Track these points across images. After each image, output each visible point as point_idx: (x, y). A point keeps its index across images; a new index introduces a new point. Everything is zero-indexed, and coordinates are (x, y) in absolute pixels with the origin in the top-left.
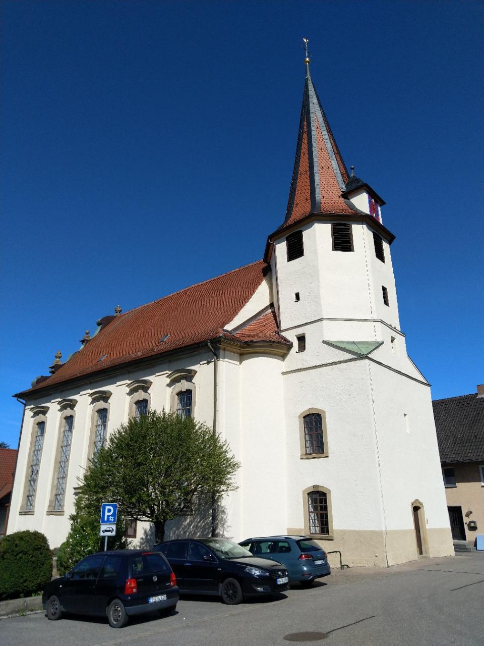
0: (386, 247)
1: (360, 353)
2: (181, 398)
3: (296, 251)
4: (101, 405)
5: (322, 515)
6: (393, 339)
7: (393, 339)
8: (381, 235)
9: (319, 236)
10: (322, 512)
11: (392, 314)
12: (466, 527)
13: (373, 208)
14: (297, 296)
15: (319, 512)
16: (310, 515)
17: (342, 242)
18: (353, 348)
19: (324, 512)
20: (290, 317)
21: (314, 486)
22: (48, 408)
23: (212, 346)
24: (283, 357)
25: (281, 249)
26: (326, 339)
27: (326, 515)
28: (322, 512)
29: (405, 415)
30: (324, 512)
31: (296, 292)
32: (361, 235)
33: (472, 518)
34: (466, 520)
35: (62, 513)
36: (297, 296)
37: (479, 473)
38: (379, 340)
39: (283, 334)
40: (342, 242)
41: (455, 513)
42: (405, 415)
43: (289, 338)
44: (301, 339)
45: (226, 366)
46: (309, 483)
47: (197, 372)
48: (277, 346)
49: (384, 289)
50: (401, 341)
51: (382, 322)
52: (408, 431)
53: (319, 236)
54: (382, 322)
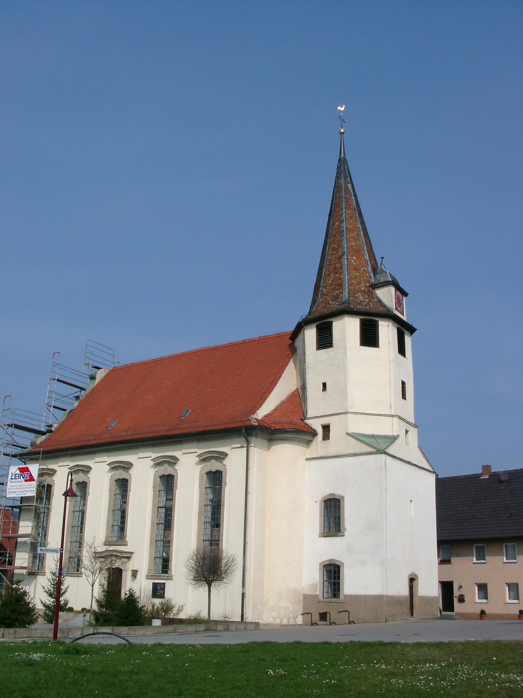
0: (408, 339)
1: (379, 445)
2: (213, 478)
3: (325, 341)
4: (121, 474)
5: (335, 583)
6: (407, 432)
7: (407, 432)
8: (404, 329)
9: (347, 328)
10: (335, 581)
11: (408, 408)
12: (456, 600)
13: (399, 303)
14: (324, 385)
15: (333, 581)
16: (324, 584)
17: (369, 338)
18: (370, 440)
19: (337, 581)
20: (316, 408)
21: (329, 560)
22: (54, 471)
23: (247, 432)
24: (309, 442)
25: (310, 335)
26: (350, 431)
27: (339, 583)
28: (335, 581)
29: (411, 501)
30: (337, 581)
31: (323, 382)
32: (387, 331)
33: (462, 592)
34: (456, 593)
35: (43, 574)
36: (324, 385)
37: (473, 551)
38: (395, 434)
39: (307, 421)
40: (369, 338)
41: (447, 587)
42: (411, 501)
43: (314, 427)
44: (326, 428)
45: (257, 451)
46: (326, 557)
47: (227, 455)
48: (302, 433)
49: (403, 383)
50: (413, 433)
51: (399, 417)
52: (412, 515)
53: (347, 328)
54: (399, 417)
